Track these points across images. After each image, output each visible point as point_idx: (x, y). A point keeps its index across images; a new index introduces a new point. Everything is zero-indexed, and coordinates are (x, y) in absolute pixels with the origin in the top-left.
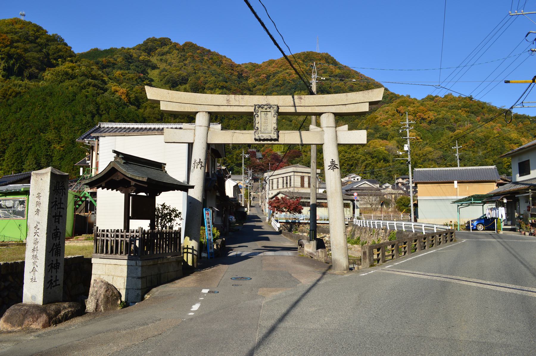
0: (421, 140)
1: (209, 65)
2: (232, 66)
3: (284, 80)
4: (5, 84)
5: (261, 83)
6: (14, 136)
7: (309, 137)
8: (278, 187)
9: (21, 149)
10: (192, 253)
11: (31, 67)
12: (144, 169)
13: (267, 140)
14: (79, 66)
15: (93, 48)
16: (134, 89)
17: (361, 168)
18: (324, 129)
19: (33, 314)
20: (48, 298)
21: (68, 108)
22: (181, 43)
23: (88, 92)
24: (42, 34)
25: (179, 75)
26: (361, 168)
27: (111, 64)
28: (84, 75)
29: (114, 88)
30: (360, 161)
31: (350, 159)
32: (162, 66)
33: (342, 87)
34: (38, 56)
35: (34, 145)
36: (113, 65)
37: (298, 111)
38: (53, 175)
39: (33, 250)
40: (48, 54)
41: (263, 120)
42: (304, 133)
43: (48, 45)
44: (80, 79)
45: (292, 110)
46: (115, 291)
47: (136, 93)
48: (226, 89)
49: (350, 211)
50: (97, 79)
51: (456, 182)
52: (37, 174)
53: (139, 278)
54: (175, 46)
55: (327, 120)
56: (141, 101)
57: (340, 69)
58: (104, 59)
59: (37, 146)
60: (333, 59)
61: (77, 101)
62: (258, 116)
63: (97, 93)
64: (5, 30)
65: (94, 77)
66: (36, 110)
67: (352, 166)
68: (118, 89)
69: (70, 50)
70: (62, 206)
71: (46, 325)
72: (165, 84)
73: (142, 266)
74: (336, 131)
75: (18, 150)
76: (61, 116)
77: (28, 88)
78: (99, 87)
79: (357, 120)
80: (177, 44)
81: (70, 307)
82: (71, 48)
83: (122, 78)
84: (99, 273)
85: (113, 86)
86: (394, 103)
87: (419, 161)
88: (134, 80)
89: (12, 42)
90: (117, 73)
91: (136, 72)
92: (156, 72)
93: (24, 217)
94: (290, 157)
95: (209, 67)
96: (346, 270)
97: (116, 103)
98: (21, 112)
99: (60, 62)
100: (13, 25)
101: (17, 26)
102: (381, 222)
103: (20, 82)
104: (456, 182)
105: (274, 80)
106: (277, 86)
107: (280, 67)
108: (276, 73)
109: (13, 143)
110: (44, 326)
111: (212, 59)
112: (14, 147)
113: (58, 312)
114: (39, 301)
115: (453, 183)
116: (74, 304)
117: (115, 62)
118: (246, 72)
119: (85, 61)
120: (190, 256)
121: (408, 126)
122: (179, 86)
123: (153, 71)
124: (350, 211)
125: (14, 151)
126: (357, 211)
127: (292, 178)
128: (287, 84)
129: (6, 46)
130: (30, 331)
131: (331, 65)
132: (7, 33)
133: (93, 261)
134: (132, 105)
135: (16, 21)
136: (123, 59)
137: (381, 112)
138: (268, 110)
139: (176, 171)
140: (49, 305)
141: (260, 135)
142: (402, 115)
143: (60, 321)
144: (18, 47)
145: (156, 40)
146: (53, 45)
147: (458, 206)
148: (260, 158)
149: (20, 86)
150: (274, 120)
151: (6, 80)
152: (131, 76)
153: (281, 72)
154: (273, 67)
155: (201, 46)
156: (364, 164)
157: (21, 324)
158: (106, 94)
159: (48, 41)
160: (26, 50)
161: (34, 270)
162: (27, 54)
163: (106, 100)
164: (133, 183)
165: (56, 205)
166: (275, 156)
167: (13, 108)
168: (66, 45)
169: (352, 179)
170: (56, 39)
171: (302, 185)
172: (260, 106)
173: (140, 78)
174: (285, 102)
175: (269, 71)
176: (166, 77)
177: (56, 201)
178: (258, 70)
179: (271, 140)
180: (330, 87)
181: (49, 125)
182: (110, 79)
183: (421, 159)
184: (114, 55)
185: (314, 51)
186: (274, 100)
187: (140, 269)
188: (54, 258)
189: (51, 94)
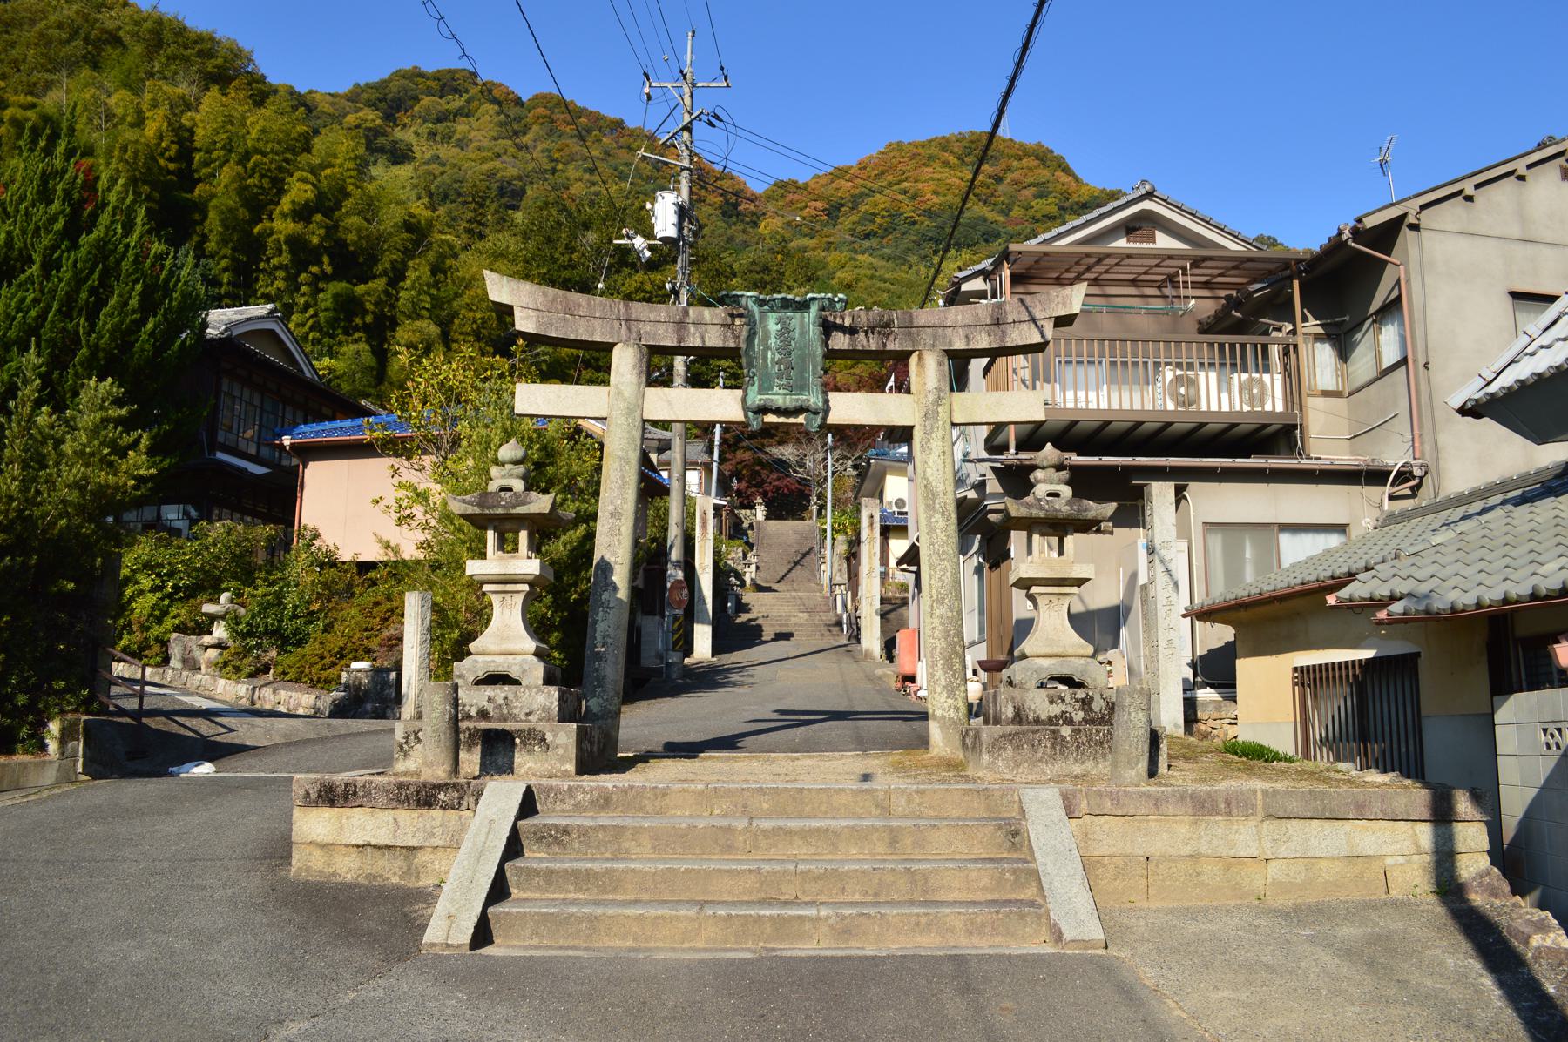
3: (894, 214)
5: (805, 230)
25: (491, 175)
32: (423, 150)
92: (404, 172)
105: (854, 218)
108: (862, 195)
145: (422, 75)
155: (592, 107)
175: (837, 189)
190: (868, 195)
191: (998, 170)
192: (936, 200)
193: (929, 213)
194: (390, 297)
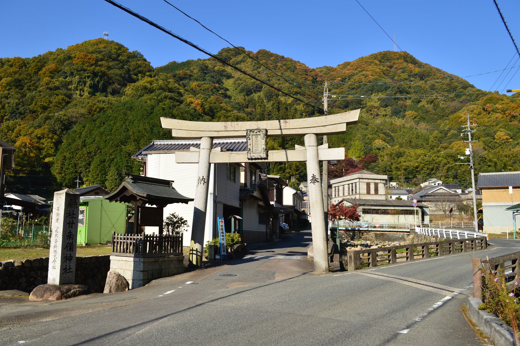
0: (511, 140)
1: (282, 71)
2: (306, 71)
3: (360, 82)
4: (90, 101)
5: (336, 86)
6: (99, 149)
7: (294, 155)
8: (344, 194)
9: (104, 161)
10: (197, 254)
11: (114, 83)
12: (150, 186)
13: (258, 159)
14: (157, 80)
15: (171, 61)
16: (209, 100)
17: (442, 172)
18: (307, 148)
19: (50, 290)
20: (63, 281)
21: (147, 121)
22: (255, 51)
23: (165, 105)
24: (124, 52)
26: (442, 172)
27: (188, 76)
28: (161, 88)
29: (190, 99)
30: (442, 164)
31: (430, 163)
33: (423, 86)
34: (120, 72)
35: (116, 157)
36: (190, 77)
37: (283, 133)
38: (67, 194)
39: (54, 247)
40: (129, 70)
41: (254, 142)
42: (289, 152)
43: (129, 62)
44: (158, 92)
45: (278, 132)
46: (124, 281)
47: (211, 103)
48: (301, 95)
49: (418, 218)
50: (173, 92)
51: (510, 188)
52: (57, 194)
53: (141, 271)
54: (249, 54)
55: (310, 140)
56: (215, 111)
57: (420, 67)
58: (181, 71)
59: (118, 157)
60: (412, 58)
61: (154, 114)
62: (250, 139)
63: (173, 105)
64: (91, 50)
65: (170, 90)
66: (118, 124)
67: (432, 170)
68: (193, 100)
69: (149, 65)
70: (74, 216)
71: (60, 298)
72: (240, 92)
73: (144, 262)
74: (317, 150)
75: (101, 162)
76: (140, 128)
77: (111, 104)
78: (175, 99)
79: (440, 120)
80: (251, 52)
81: (79, 287)
82: (150, 63)
83: (199, 88)
84: (115, 267)
85: (188, 98)
86: (480, 101)
87: (509, 163)
88: (210, 90)
89: (97, 60)
90: (193, 84)
91: (211, 83)
92: (231, 81)
93: (83, 224)
94: (365, 162)
95: (282, 74)
96: (326, 271)
97: (191, 115)
98: (104, 126)
99: (140, 77)
100: (97, 45)
101: (101, 46)
102: (451, 231)
103: (104, 98)
104: (510, 188)
105: (350, 83)
106: (353, 89)
107: (356, 69)
108: (352, 75)
109: (98, 156)
110: (57, 299)
111: (286, 65)
112: (98, 159)
113: (69, 290)
114: (57, 282)
115: (508, 188)
116: (83, 286)
117: (191, 73)
118: (321, 76)
119: (162, 75)
120: (195, 256)
121: (469, 129)
122: (254, 94)
123: (228, 80)
124: (418, 218)
125: (99, 163)
126: (427, 219)
127: (358, 186)
128: (363, 86)
129: (92, 65)
130: (47, 301)
131: (410, 64)
132: (93, 53)
133: (111, 258)
134: (207, 115)
135: (101, 41)
136: (199, 71)
137: (466, 111)
138: (258, 133)
139: (181, 188)
140: (64, 286)
141: (252, 155)
142: (489, 113)
143: (70, 297)
144: (102, 65)
146: (134, 61)
147: (514, 213)
148: (335, 164)
149: (104, 102)
150: (263, 142)
151: (91, 97)
152: (207, 86)
153: (357, 74)
154: (349, 70)
156: (445, 168)
157: (42, 297)
158: (182, 106)
159: (128, 58)
160: (109, 68)
161: (54, 261)
162: (110, 72)
163: (182, 111)
164: (138, 198)
165: (69, 215)
166: (350, 161)
167: (98, 123)
168: (145, 60)
169: (433, 184)
170: (136, 56)
171: (368, 192)
172: (251, 131)
173: (215, 88)
174: (273, 126)
175: (344, 74)
176: (241, 86)
177: (70, 213)
178: (333, 73)
179: (261, 159)
180: (410, 87)
181: (128, 138)
182: (186, 91)
183: (511, 161)
184: (190, 67)
185: (391, 50)
186: (264, 125)
187: (142, 264)
188: (68, 253)
189: (131, 108)
190: (353, 76)
191: (391, 64)
192: (372, 78)
193: (370, 82)
194: (285, 167)
